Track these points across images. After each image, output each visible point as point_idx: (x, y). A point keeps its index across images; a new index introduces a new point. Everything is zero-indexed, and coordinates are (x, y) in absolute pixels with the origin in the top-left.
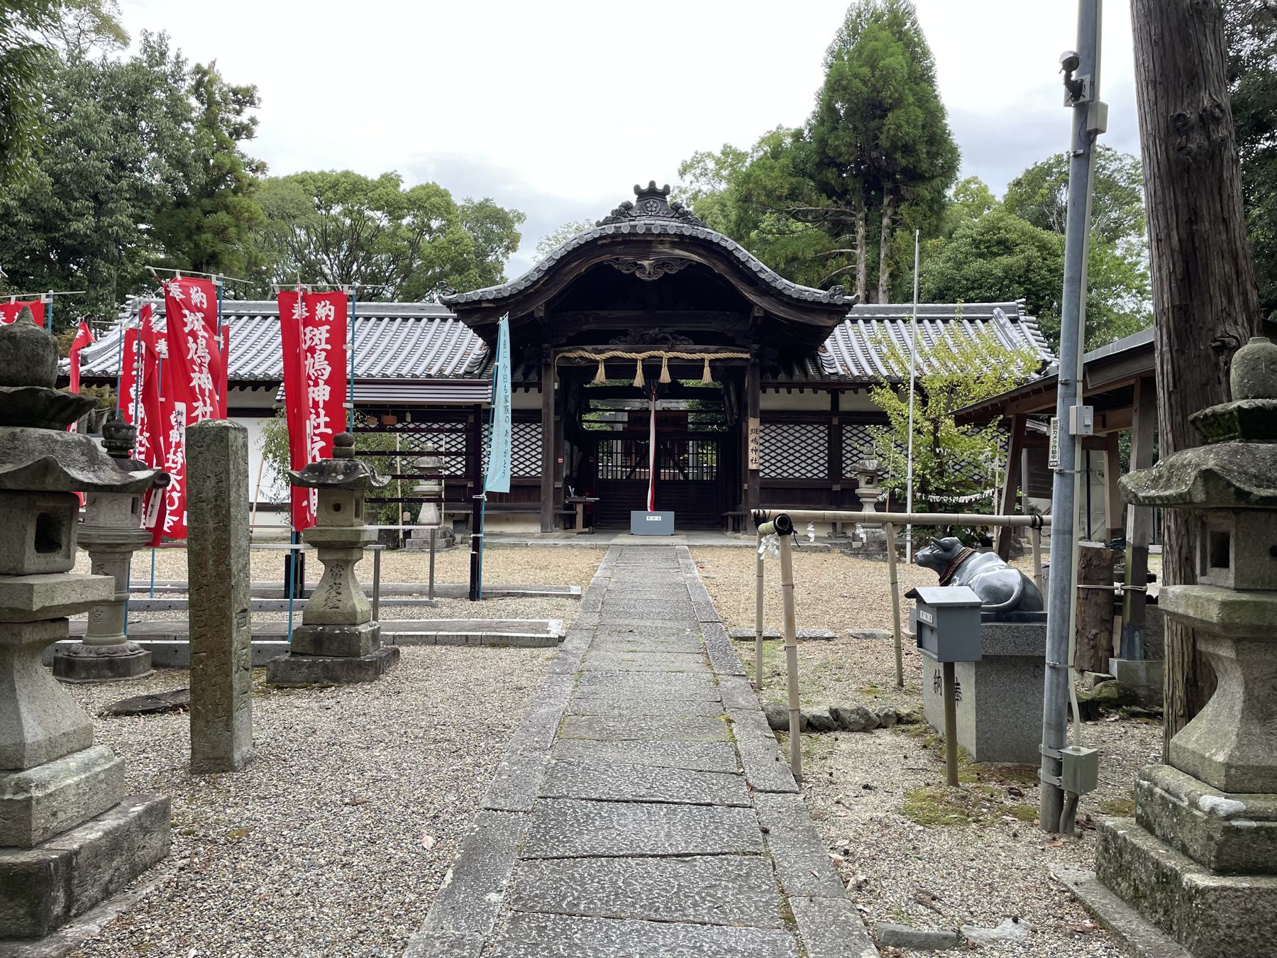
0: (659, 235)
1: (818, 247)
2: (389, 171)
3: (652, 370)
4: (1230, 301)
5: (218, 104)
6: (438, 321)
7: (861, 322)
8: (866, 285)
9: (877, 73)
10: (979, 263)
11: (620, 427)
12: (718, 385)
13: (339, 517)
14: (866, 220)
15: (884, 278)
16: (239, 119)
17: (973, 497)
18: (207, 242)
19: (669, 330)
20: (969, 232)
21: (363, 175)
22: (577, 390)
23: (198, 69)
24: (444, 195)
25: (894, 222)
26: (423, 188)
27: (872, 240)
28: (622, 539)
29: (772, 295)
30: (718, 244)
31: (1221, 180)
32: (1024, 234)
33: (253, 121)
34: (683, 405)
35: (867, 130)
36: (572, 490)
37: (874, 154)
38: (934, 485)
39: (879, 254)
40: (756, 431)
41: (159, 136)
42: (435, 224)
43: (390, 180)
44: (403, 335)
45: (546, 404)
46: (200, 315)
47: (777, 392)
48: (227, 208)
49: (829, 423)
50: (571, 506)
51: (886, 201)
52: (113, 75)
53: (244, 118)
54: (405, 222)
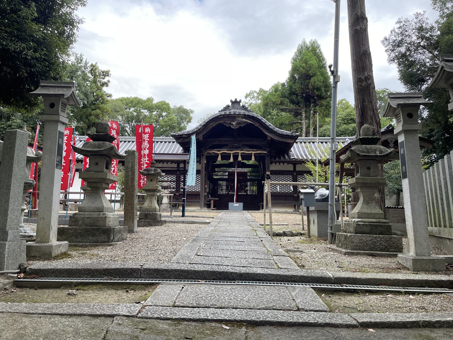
0: (238, 115)
1: (290, 120)
3: (236, 157)
4: (372, 120)
5: (97, 76)
6: (167, 142)
7: (303, 143)
8: (306, 132)
9: (308, 66)
10: (344, 126)
12: (257, 163)
13: (152, 183)
15: (311, 130)
16: (104, 81)
19: (241, 144)
20: (341, 116)
23: (92, 65)
24: (168, 104)
25: (315, 112)
26: (160, 102)
27: (307, 118)
31: (370, 93)
33: (109, 81)
34: (246, 170)
37: (307, 91)
41: (79, 85)
42: (164, 114)
43: (150, 100)
45: (202, 167)
46: (115, 131)
48: (99, 108)
49: (293, 174)
51: (312, 105)
53: (106, 80)
54: (154, 113)
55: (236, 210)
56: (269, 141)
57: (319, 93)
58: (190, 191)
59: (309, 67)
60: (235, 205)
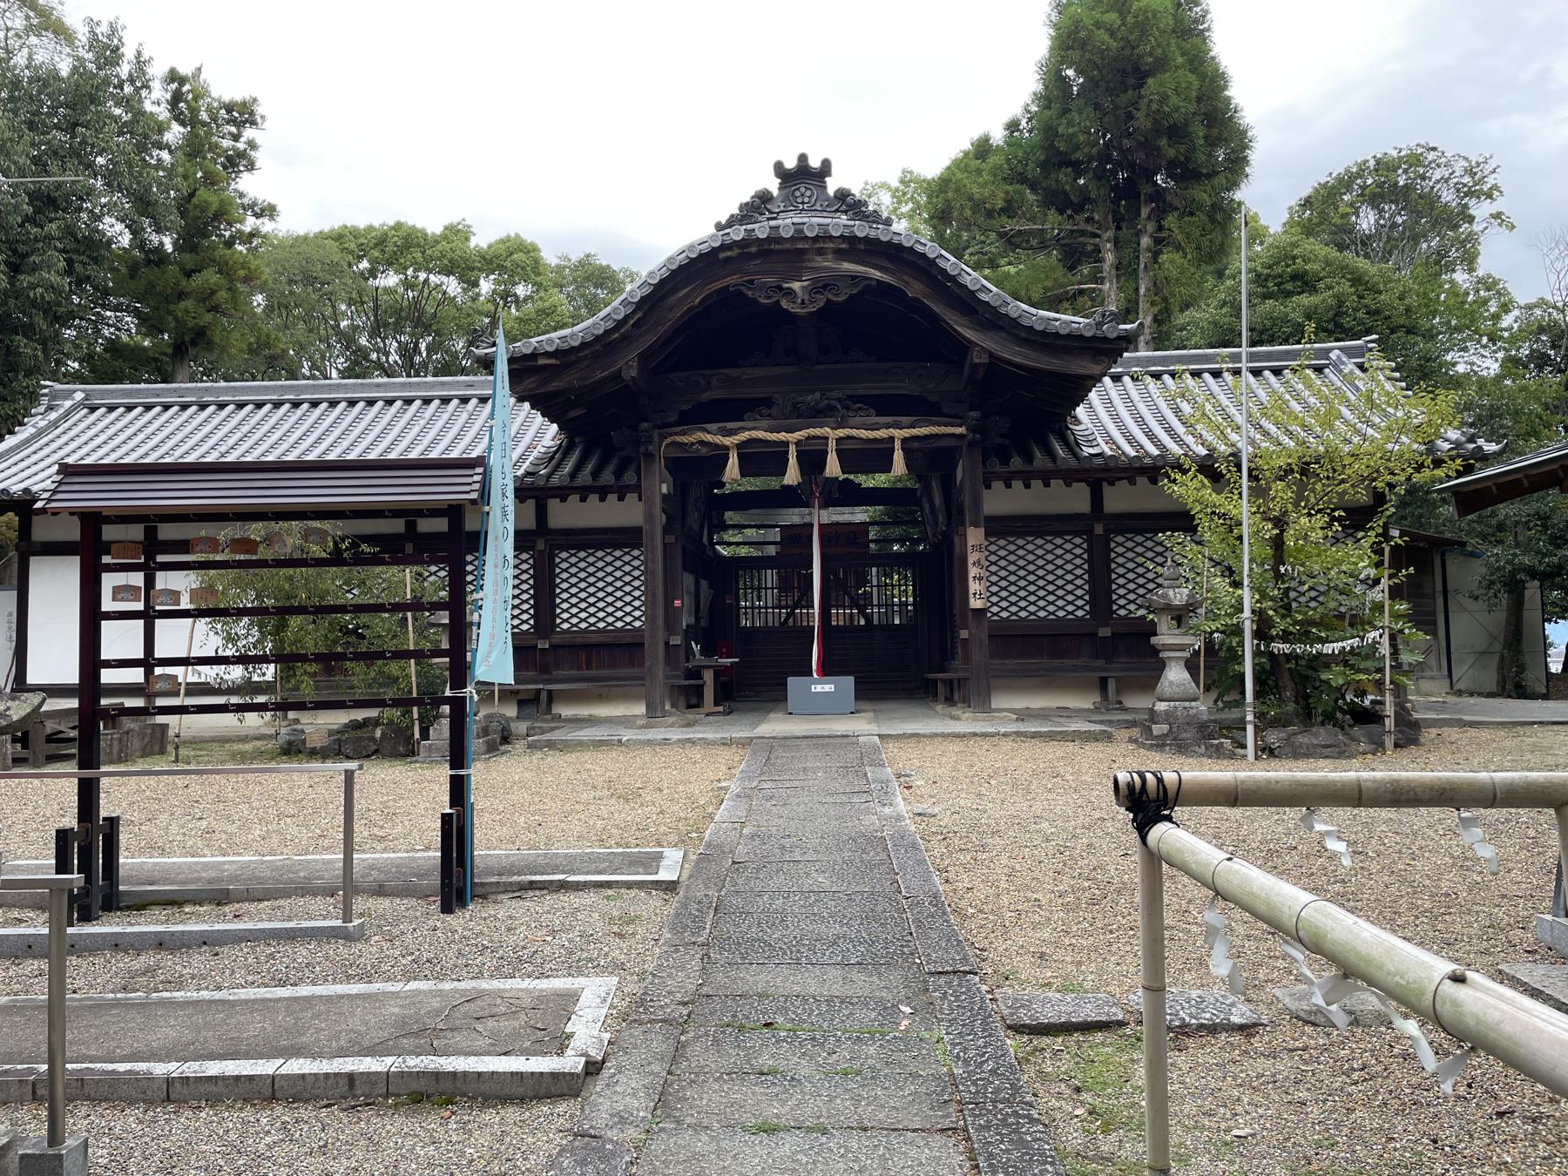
0: (816, 239)
1: (1049, 283)
2: (455, 221)
3: (812, 459)
5: (204, 124)
9: (1130, 19)
11: (772, 551)
14: (1117, 243)
17: (1347, 644)
18: (187, 311)
19: (836, 394)
21: (419, 226)
22: (698, 498)
24: (530, 250)
25: (1158, 241)
26: (502, 241)
27: (1126, 270)
28: (774, 726)
29: (1001, 328)
30: (911, 249)
32: (1328, 263)
33: (252, 145)
34: (860, 515)
35: (1116, 107)
36: (696, 648)
38: (1280, 624)
39: (1137, 289)
40: (979, 548)
42: (521, 290)
43: (457, 233)
44: (440, 424)
45: (649, 517)
47: (1008, 486)
50: (696, 673)
51: (1145, 212)
52: (46, 80)
55: (821, 708)
56: (981, 371)
57: (1182, 148)
58: (603, 630)
59: (1137, 24)
60: (818, 688)
